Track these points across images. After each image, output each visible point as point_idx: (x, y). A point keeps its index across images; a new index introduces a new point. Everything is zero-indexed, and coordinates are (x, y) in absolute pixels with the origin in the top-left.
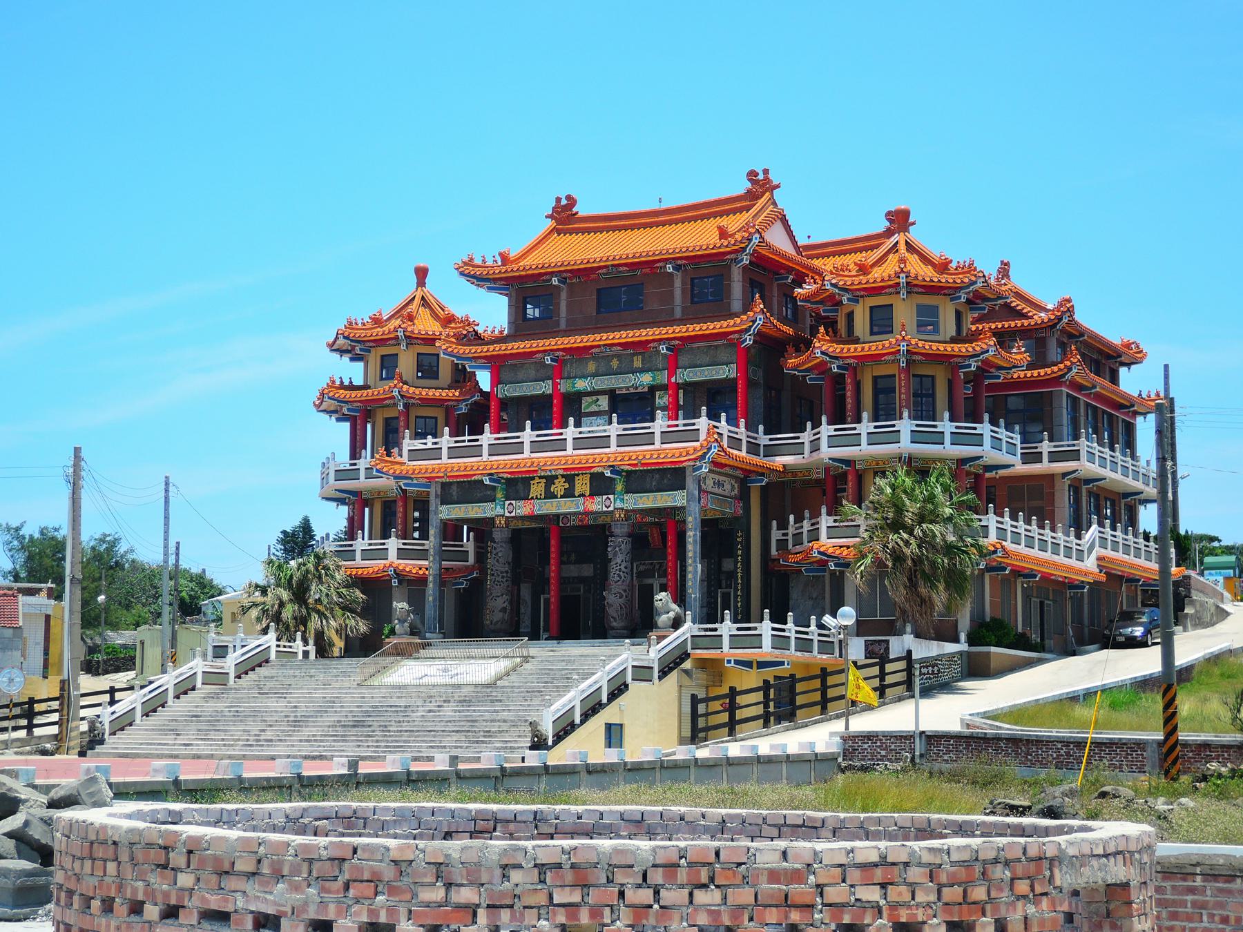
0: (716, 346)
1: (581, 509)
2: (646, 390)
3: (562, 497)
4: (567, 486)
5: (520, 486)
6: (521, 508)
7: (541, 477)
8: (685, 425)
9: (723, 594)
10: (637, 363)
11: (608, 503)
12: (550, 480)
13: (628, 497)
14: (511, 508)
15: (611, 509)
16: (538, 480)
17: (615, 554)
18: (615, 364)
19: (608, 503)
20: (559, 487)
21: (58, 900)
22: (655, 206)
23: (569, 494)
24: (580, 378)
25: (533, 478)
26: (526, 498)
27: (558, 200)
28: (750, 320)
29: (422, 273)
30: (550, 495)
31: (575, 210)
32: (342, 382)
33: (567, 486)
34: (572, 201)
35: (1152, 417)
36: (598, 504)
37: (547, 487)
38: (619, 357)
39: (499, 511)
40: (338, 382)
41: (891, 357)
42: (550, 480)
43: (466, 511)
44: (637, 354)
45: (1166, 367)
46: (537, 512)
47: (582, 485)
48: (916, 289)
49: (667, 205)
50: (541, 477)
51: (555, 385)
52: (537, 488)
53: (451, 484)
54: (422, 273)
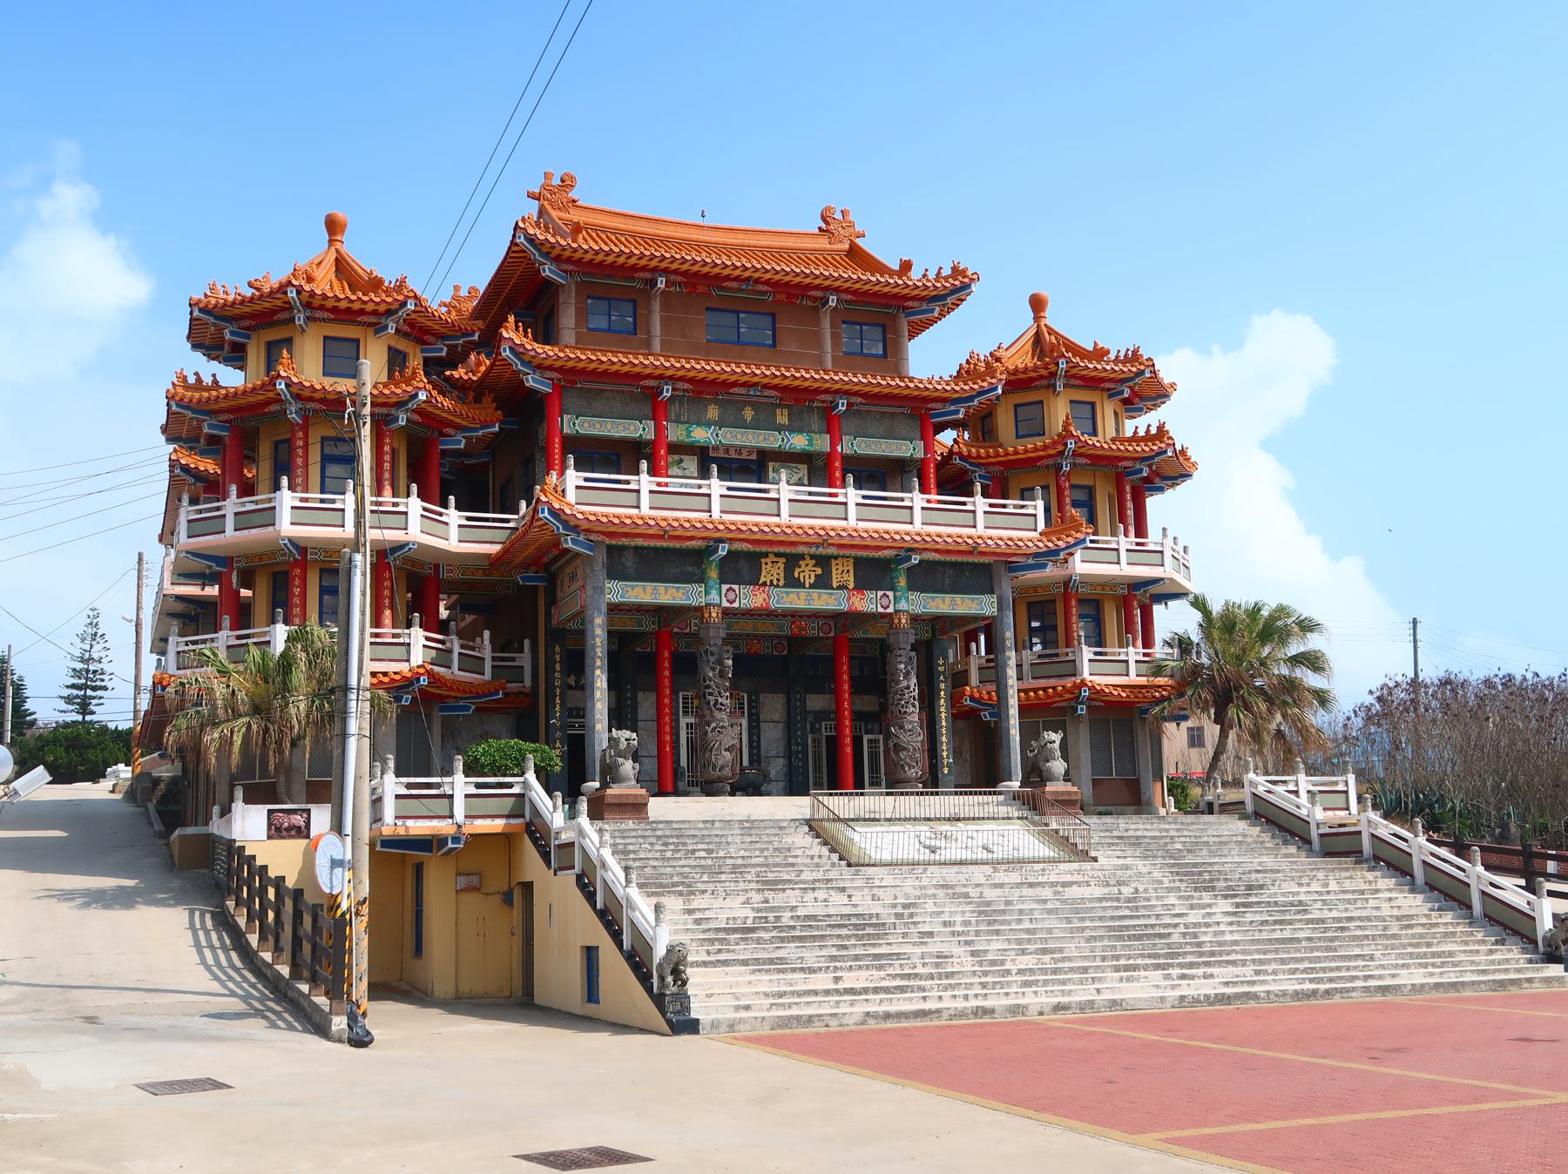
0: (892, 414)
1: (844, 607)
2: (754, 457)
3: (812, 586)
4: (819, 571)
5: (743, 565)
6: (747, 598)
7: (777, 555)
8: (1015, 507)
9: (870, 741)
10: (782, 418)
11: (885, 602)
12: (792, 561)
13: (913, 596)
14: (731, 596)
15: (890, 610)
16: (772, 558)
17: (907, 675)
18: (748, 414)
19: (885, 602)
20: (808, 572)
21: (1035, 774)
22: (700, 221)
23: (823, 582)
24: (699, 424)
25: (766, 555)
26: (754, 581)
27: (547, 175)
28: (549, 351)
29: (1037, 304)
30: (792, 582)
31: (573, 194)
32: (199, 380)
33: (819, 571)
34: (567, 182)
35: (327, 1009)
36: (870, 602)
37: (789, 571)
38: (755, 406)
39: (714, 596)
40: (192, 380)
41: (1050, 462)
42: (824, 562)
43: (655, 592)
44: (781, 406)
45: (1415, 622)
46: (774, 604)
47: (842, 573)
48: (319, 314)
49: (707, 222)
50: (777, 555)
51: (659, 430)
52: (772, 571)
53: (623, 548)
54: (1037, 304)
